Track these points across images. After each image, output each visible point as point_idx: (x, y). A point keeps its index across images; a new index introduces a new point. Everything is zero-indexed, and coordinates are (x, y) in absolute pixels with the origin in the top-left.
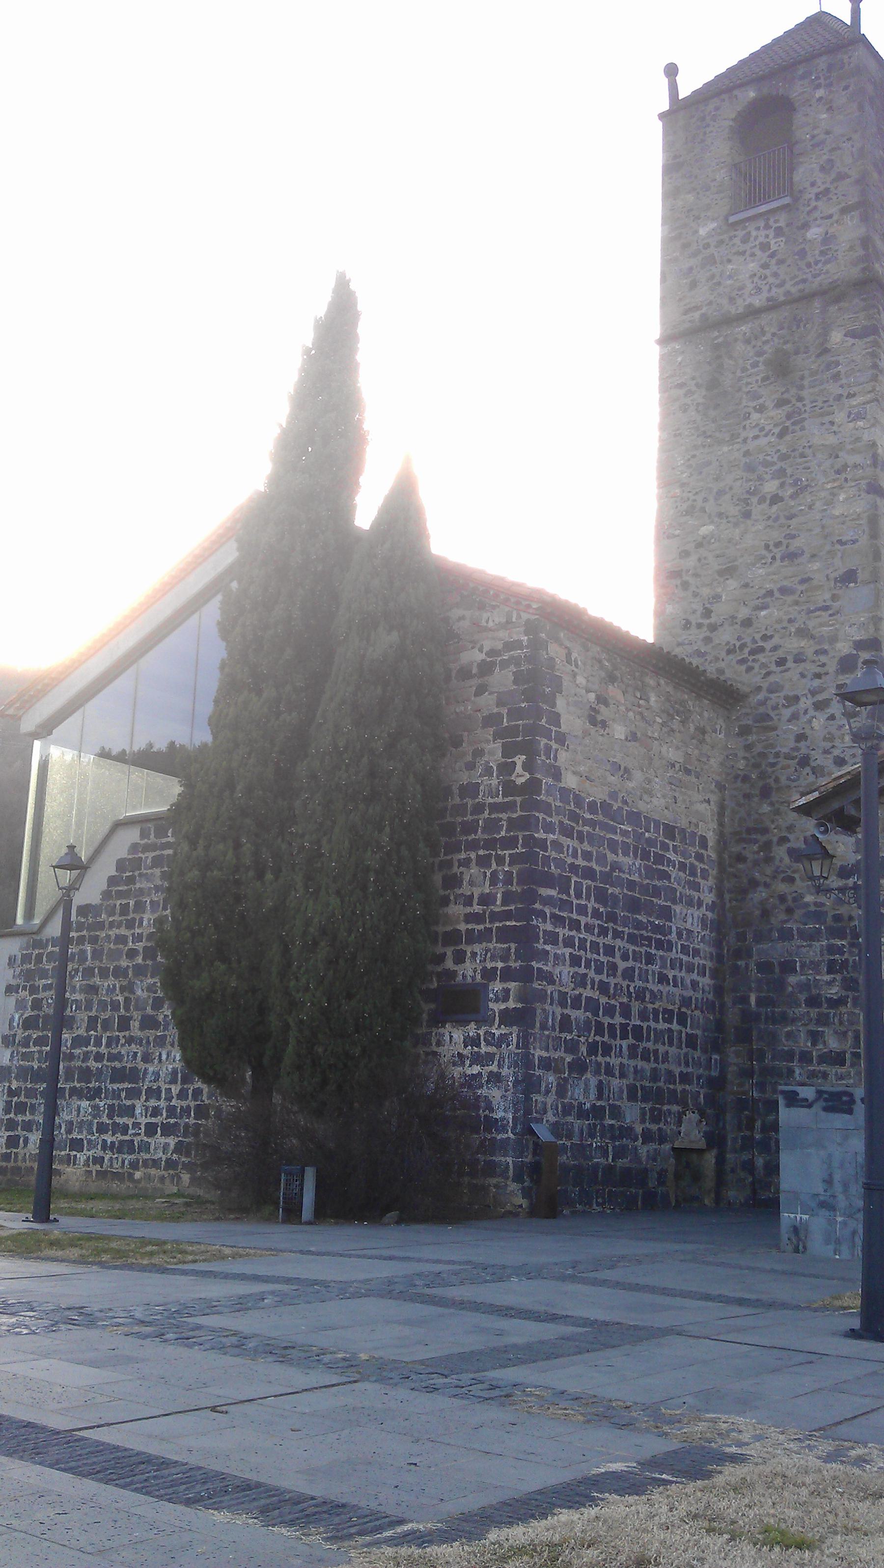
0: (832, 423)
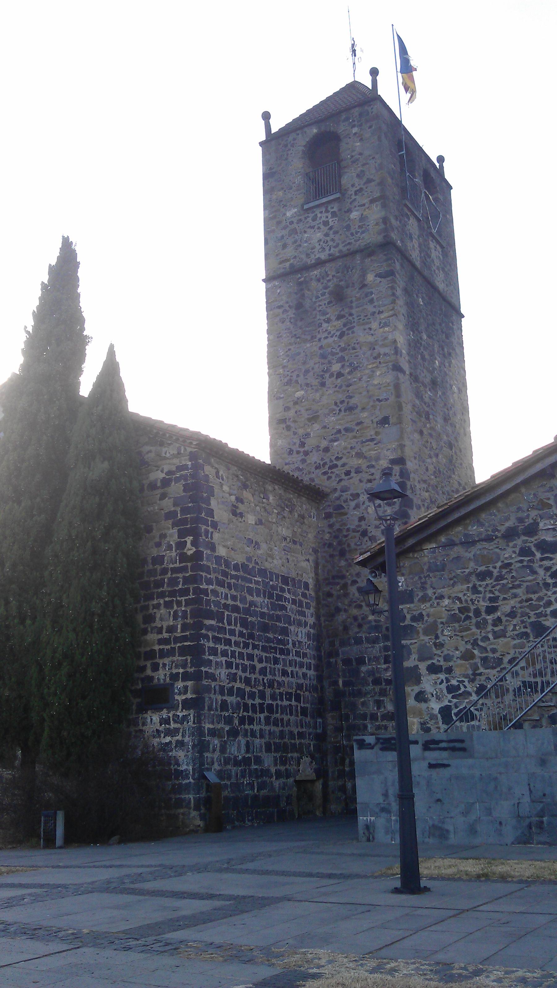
0: (370, 329)
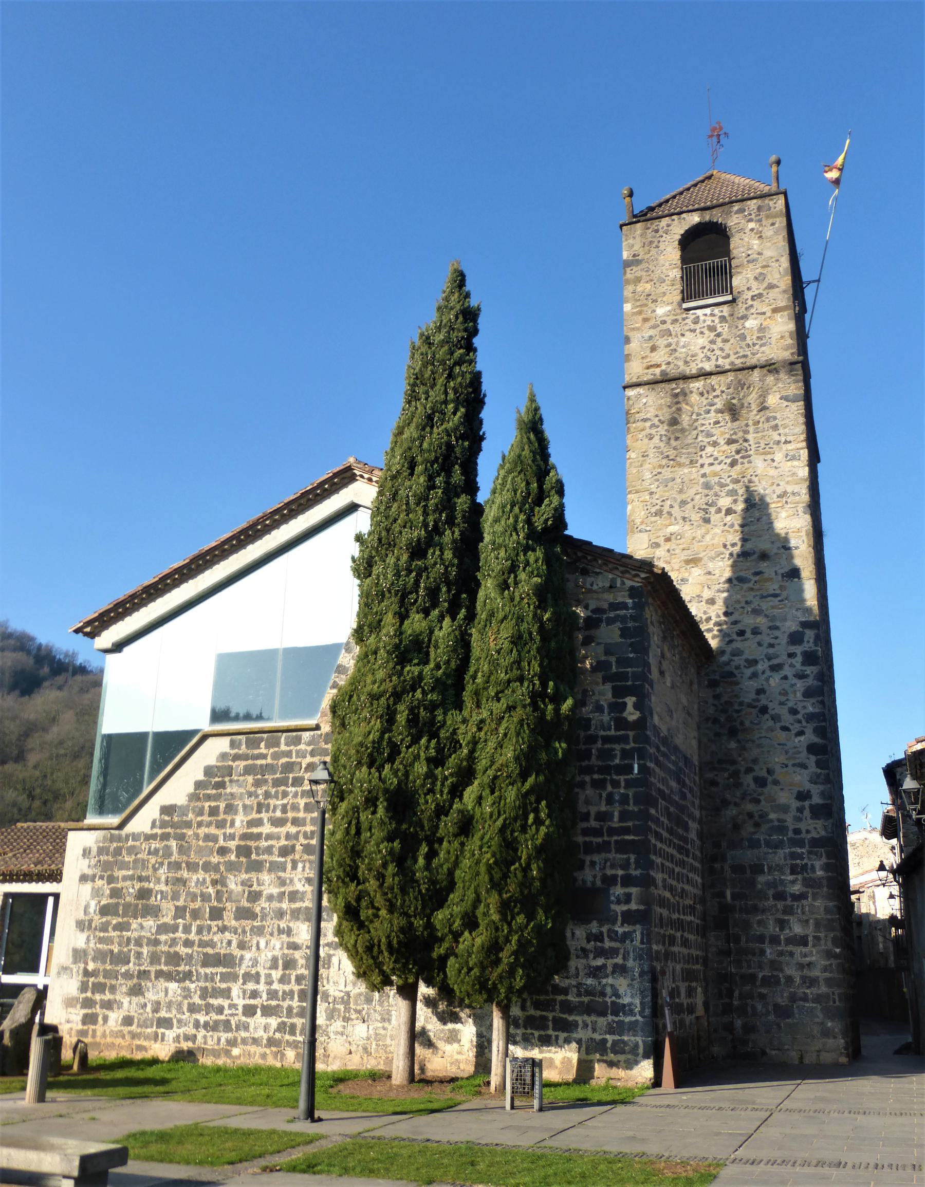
0: (773, 460)
